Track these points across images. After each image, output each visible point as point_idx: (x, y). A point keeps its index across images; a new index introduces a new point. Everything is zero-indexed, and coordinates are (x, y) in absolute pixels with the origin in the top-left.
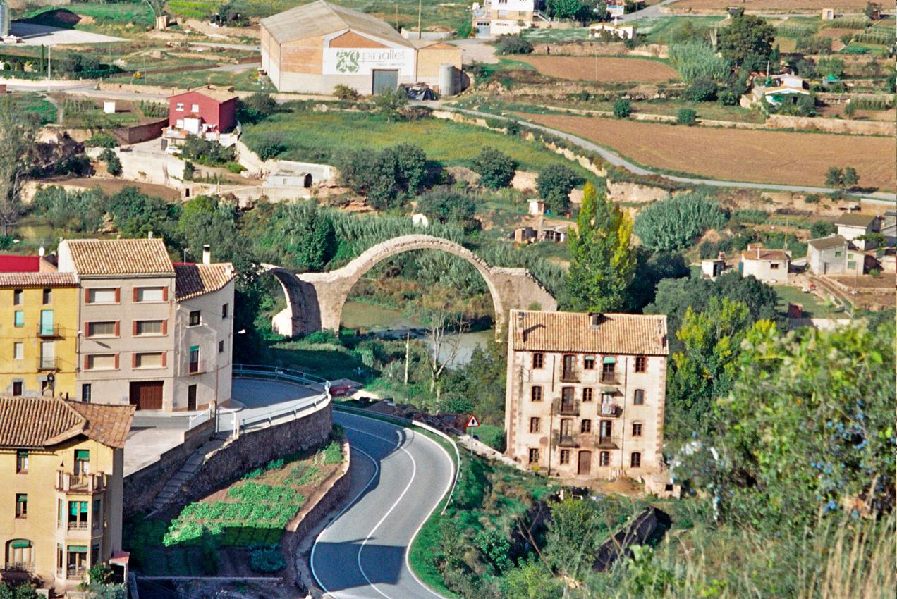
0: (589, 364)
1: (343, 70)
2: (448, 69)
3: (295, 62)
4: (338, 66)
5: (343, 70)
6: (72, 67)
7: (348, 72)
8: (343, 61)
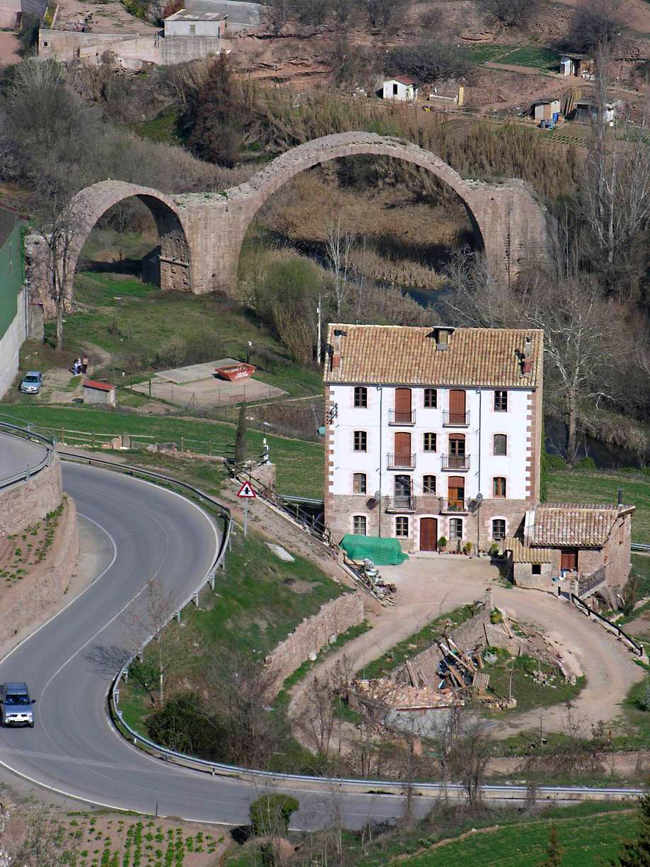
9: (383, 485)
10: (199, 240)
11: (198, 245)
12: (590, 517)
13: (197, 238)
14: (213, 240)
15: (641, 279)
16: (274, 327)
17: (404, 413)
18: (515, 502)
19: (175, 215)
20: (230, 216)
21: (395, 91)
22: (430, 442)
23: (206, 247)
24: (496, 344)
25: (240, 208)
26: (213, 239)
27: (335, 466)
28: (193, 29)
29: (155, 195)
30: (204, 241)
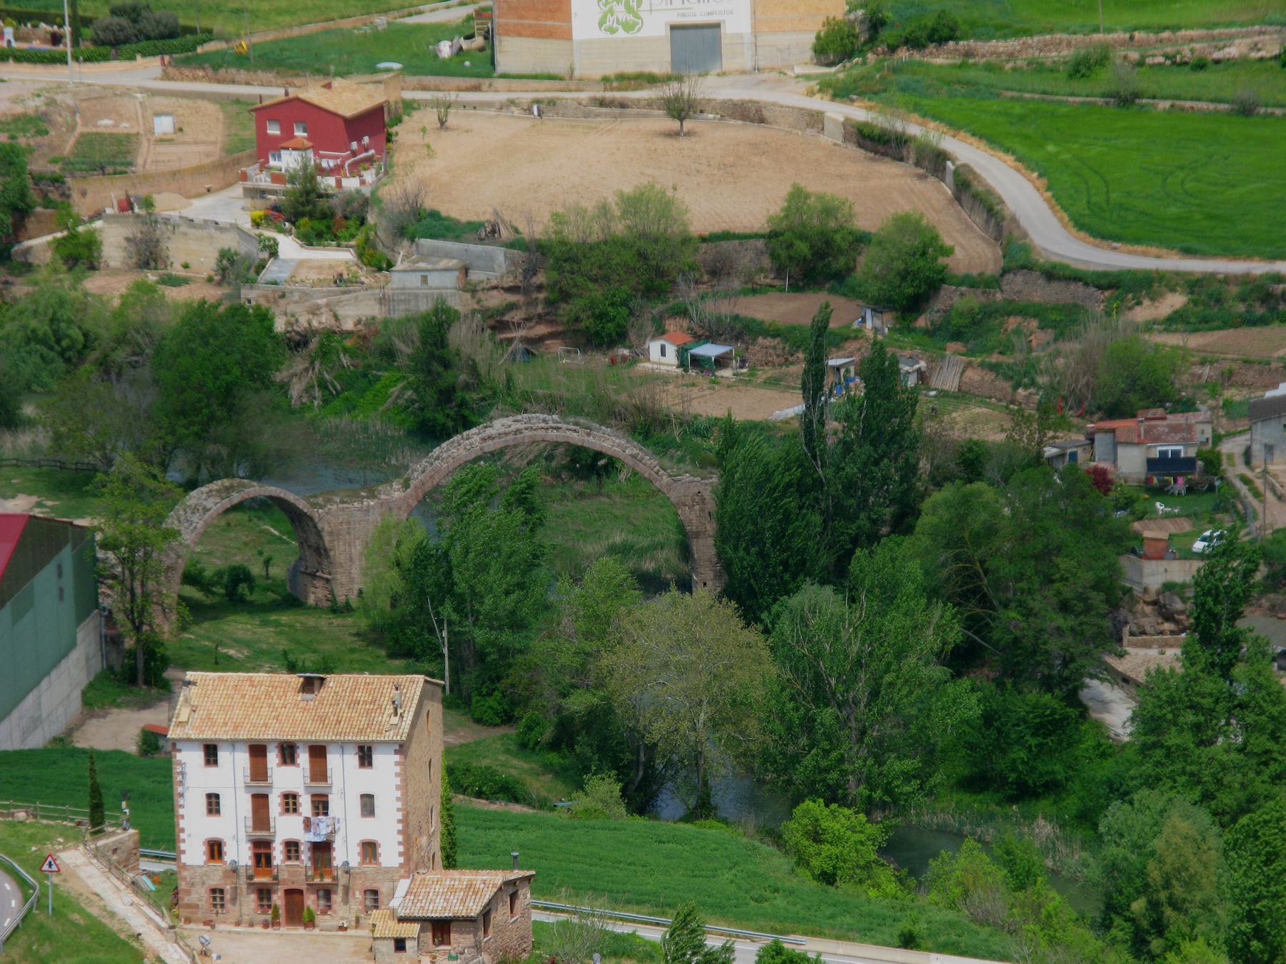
0: (263, 860)
1: (612, 31)
2: (648, 598)
3: (521, 17)
4: (601, 24)
5: (612, 31)
6: (842, 416)
7: (621, 34)
8: (611, 11)
9: (240, 853)
12: (470, 886)
17: (259, 773)
18: (388, 870)
19: (311, 519)
21: (663, 353)
22: (290, 802)
25: (390, 509)
26: (358, 547)
27: (187, 832)
28: (425, 279)
29: (282, 495)
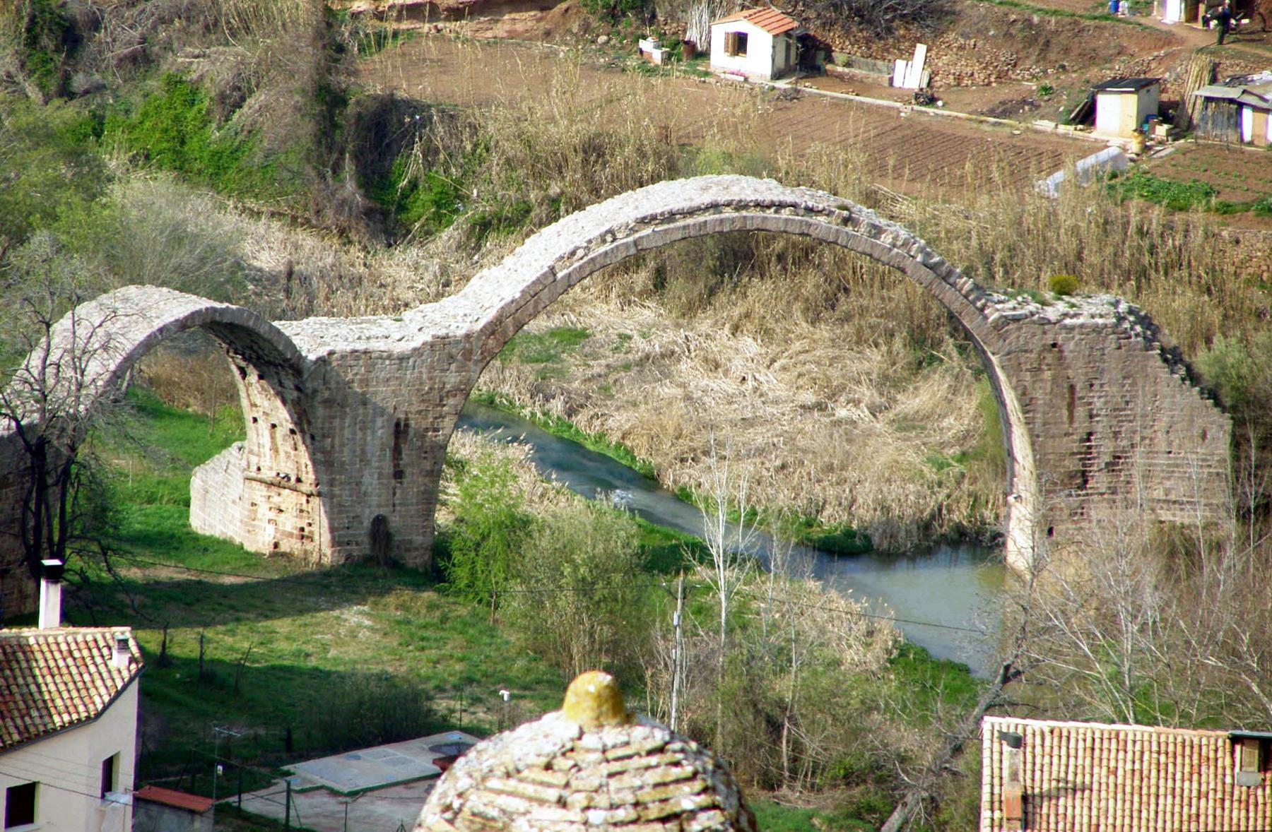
10: (347, 433)
11: (343, 445)
13: (342, 429)
14: (380, 432)
15: (423, 493)
16: (332, 593)
20: (425, 376)
23: (363, 451)
24: (1064, 739)
30: (360, 435)
